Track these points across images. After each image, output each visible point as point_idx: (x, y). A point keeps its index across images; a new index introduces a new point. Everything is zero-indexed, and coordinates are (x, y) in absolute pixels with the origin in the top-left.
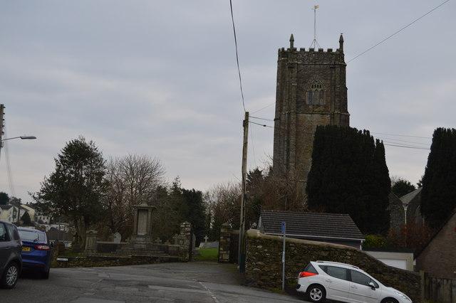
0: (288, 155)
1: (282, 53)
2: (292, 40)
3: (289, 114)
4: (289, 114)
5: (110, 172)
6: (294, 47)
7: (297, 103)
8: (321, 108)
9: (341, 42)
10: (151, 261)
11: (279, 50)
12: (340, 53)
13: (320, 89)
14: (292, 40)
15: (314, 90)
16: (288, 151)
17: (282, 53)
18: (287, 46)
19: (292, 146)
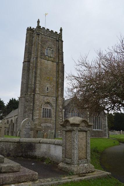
0: (35, 80)
1: (30, 30)
2: (38, 22)
3: (37, 58)
4: (37, 58)
5: (30, 166)
6: (40, 25)
7: (41, 53)
8: (52, 59)
9: (61, 30)
10: (9, 172)
11: (28, 28)
12: (61, 35)
13: (51, 49)
14: (38, 22)
15: (49, 49)
16: (35, 77)
17: (30, 30)
18: (34, 26)
19: (38, 75)
